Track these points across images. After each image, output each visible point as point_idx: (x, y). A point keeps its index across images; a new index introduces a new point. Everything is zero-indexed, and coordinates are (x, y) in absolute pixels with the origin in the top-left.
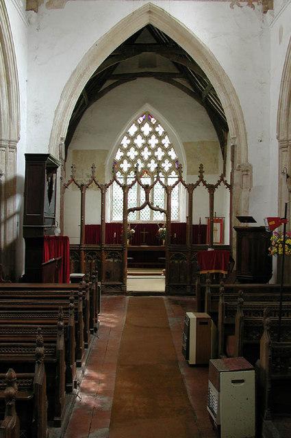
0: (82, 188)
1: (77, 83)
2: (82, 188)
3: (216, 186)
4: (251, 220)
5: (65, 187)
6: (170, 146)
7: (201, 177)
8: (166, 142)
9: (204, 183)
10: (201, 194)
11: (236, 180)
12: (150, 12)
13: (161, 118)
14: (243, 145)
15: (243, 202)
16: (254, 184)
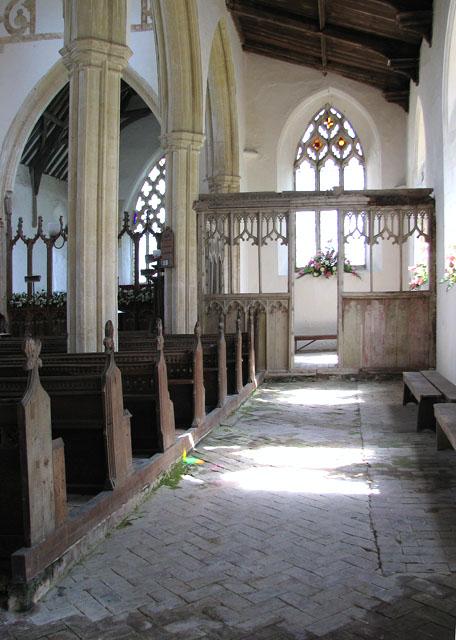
0: (30, 243)
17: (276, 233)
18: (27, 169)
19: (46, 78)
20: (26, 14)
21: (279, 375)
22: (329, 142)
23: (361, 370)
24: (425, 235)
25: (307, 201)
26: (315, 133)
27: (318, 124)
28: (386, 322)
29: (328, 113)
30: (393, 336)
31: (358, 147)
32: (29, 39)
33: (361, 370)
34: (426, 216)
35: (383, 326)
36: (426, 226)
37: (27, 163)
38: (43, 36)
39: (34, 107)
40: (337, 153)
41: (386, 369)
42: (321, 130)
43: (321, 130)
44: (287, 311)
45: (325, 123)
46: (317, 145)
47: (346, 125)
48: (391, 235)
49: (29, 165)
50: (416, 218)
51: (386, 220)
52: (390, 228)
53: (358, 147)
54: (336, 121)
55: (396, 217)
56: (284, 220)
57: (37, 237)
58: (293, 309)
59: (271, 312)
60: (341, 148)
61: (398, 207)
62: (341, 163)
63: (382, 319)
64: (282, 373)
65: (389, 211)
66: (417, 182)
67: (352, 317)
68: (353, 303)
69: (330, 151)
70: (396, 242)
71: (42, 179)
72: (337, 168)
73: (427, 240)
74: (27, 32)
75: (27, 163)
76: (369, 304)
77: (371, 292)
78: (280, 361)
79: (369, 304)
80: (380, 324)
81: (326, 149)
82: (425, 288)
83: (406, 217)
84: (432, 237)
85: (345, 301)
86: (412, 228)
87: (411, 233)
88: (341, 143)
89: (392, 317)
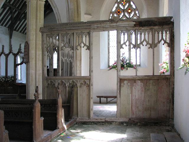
0: (7, 56)
17: (84, 43)
18: (7, 29)
21: (85, 120)
22: (124, 11)
23: (130, 119)
24: (167, 43)
25: (100, 25)
26: (118, 7)
27: (119, 3)
28: (145, 93)
30: (149, 101)
31: (137, 12)
33: (130, 119)
34: (168, 33)
35: (143, 94)
36: (168, 36)
37: (7, 26)
41: (144, 119)
42: (120, 6)
43: (120, 6)
44: (89, 86)
45: (123, 3)
47: (132, 3)
48: (148, 43)
49: (8, 27)
50: (162, 34)
51: (145, 35)
52: (147, 39)
53: (137, 12)
55: (150, 33)
56: (88, 36)
57: (10, 53)
58: (92, 85)
59: (80, 87)
60: (129, 13)
61: (152, 27)
63: (142, 91)
64: (86, 119)
65: (146, 30)
66: (165, 12)
67: (125, 90)
68: (125, 82)
69: (124, 15)
70: (151, 47)
71: (13, 32)
73: (169, 46)
75: (7, 26)
76: (135, 82)
77: (136, 75)
78: (85, 113)
79: (135, 82)
80: (141, 94)
81: (122, 14)
82: (168, 73)
83: (156, 33)
84: (172, 45)
85: (121, 81)
86: (160, 38)
87: (159, 42)
88: (130, 11)
89: (148, 90)
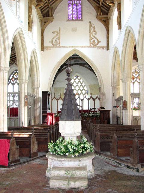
0: (57, 100)
1: (55, 71)
2: (57, 100)
3: (96, 99)
4: (104, 108)
5: (52, 99)
6: (85, 86)
7: (91, 96)
8: (83, 84)
9: (92, 98)
10: (91, 101)
11: (101, 97)
12: (75, 51)
13: (81, 77)
14: (103, 87)
15: (103, 103)
16: (106, 98)
19: (63, 57)
20: (58, 41)
22: (136, 78)
29: (136, 71)
32: (59, 47)
38: (63, 47)
39: (59, 64)
40: (12, 82)
46: (133, 78)
54: (138, 73)
62: (13, 84)
72: (12, 86)
74: (58, 45)
